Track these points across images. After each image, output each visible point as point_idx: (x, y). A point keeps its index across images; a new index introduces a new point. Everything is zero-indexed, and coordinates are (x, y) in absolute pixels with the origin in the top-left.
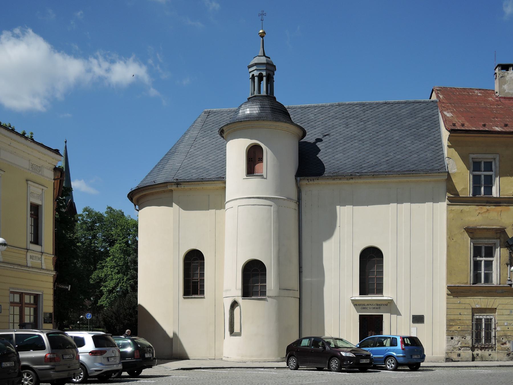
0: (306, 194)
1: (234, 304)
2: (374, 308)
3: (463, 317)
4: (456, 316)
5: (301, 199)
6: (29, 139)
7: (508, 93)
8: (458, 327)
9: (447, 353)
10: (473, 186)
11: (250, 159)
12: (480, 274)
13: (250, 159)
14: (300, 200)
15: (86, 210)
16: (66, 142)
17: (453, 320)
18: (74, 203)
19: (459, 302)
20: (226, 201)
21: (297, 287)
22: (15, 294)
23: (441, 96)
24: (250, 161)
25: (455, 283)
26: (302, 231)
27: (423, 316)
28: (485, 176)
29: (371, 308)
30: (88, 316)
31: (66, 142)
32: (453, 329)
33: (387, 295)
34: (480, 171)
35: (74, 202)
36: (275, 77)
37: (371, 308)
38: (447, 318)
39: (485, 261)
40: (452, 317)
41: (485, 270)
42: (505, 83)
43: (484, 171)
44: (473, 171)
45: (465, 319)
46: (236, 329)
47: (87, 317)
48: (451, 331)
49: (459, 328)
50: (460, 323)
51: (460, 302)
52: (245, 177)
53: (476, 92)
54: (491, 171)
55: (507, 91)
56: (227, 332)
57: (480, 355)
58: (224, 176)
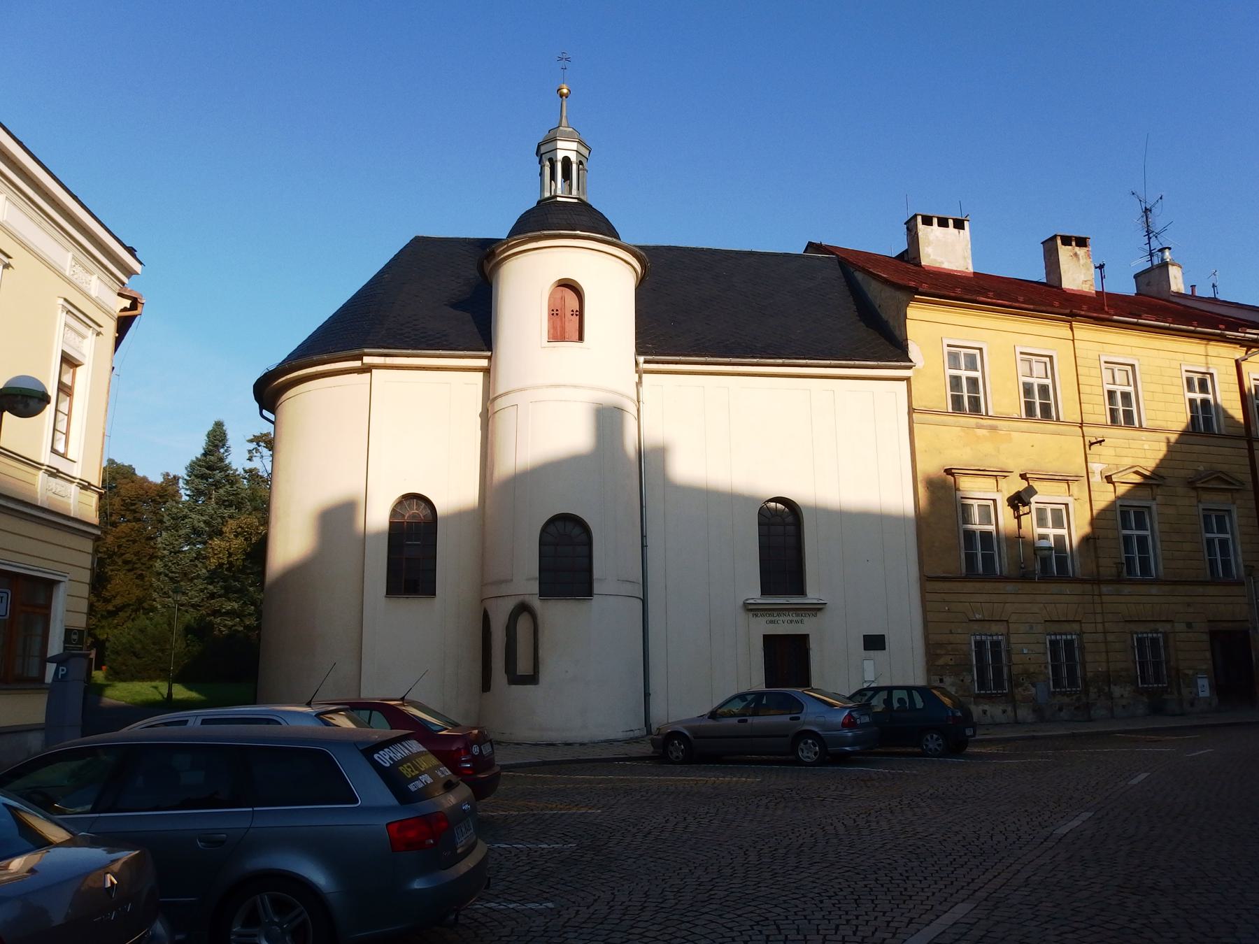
2: (791, 621)
6: (92, 487)
7: (935, 260)
8: (950, 657)
11: (553, 310)
12: (1230, 560)
19: (947, 608)
22: (1191, 294)
24: (553, 314)
27: (884, 636)
29: (786, 623)
31: (588, 349)
32: (941, 662)
37: (786, 623)
41: (1221, 556)
42: (929, 245)
46: (523, 667)
48: (938, 666)
49: (951, 660)
55: (932, 257)
57: (988, 713)
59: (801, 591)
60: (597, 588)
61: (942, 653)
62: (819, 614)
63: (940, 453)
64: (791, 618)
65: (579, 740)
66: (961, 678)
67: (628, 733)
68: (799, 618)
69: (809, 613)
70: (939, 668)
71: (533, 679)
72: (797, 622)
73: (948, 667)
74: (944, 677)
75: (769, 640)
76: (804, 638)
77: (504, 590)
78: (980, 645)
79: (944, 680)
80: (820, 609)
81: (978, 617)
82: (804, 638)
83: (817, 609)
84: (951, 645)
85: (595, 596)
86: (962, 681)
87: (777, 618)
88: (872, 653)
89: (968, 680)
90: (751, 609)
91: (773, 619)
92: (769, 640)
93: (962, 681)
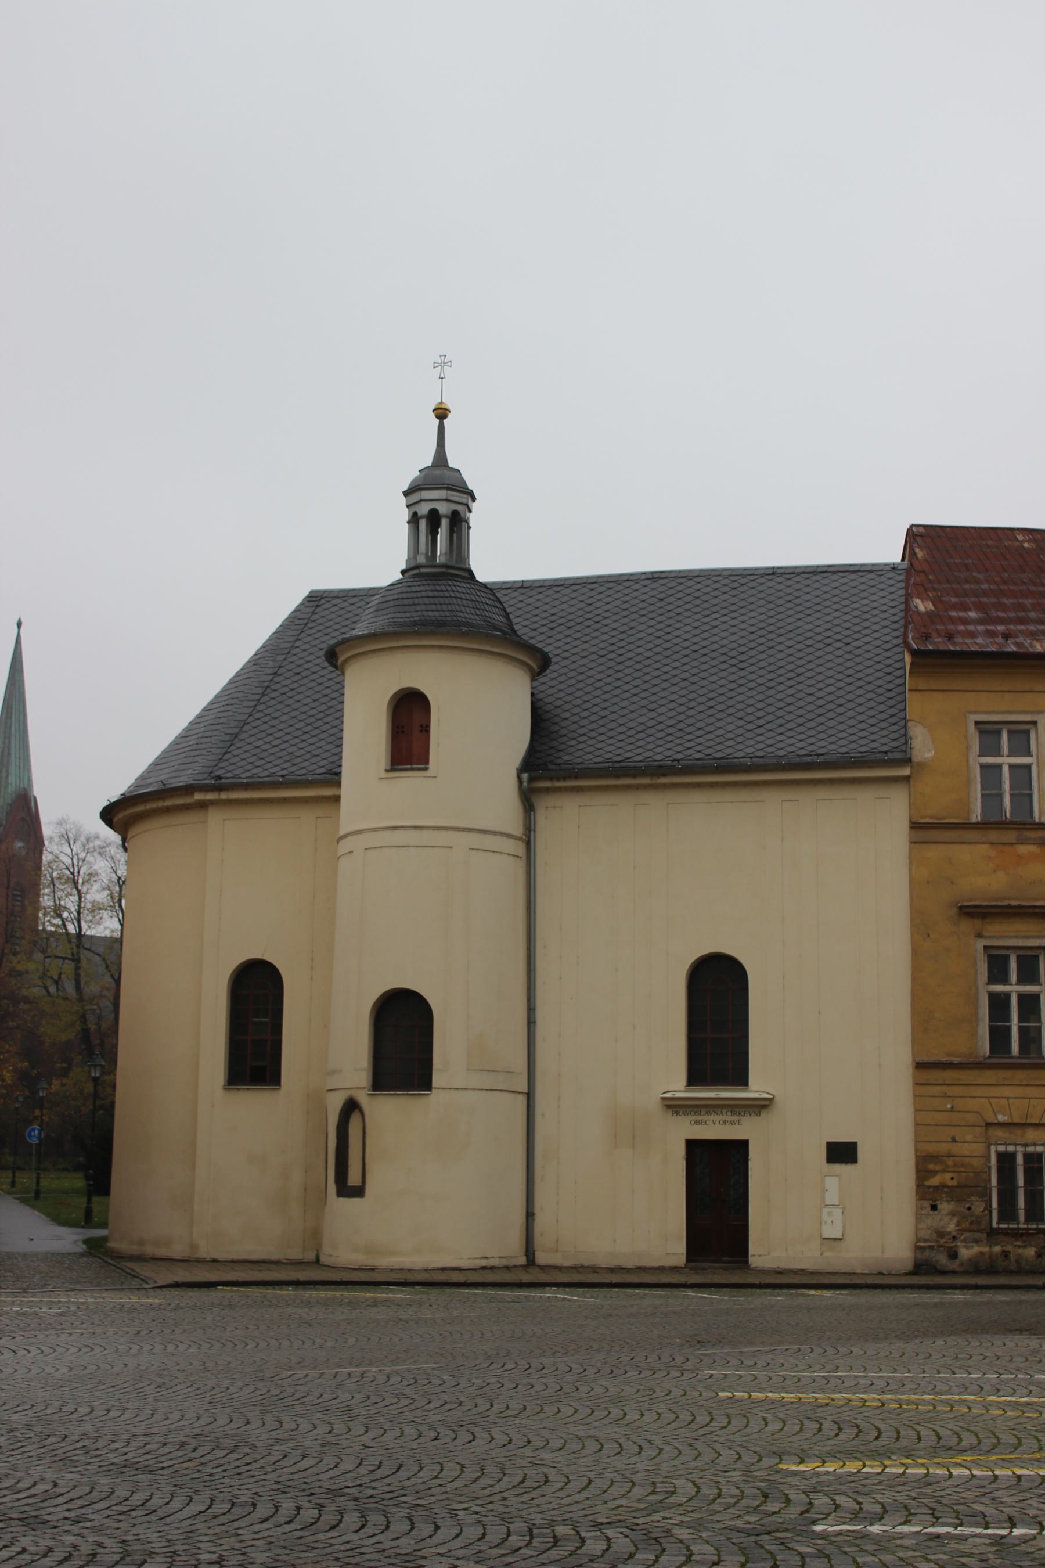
0: (546, 818)
1: (351, 1107)
2: (725, 1122)
3: (963, 1149)
4: (943, 1145)
5: (534, 831)
9: (918, 1248)
10: (1001, 789)
11: (398, 727)
13: (398, 727)
14: (532, 833)
15: (60, 823)
16: (19, 624)
17: (934, 1158)
18: (35, 798)
19: (949, 1106)
20: (342, 832)
21: (520, 1063)
23: (920, 554)
24: (398, 732)
25: (920, 1059)
26: (535, 912)
28: (1012, 767)
29: (717, 1123)
30: (33, 1134)
31: (19, 624)
32: (935, 1181)
33: (757, 1087)
34: (999, 754)
35: (35, 793)
36: (473, 519)
37: (717, 1123)
38: (916, 1151)
39: (1021, 997)
40: (932, 1148)
43: (1008, 756)
44: (979, 756)
45: (967, 1154)
46: (354, 1179)
47: (30, 1136)
48: (929, 1187)
49: (952, 1179)
50: (955, 1165)
51: (952, 1107)
52: (384, 774)
53: (1020, 537)
54: (1029, 754)
56: (332, 1188)
58: (337, 770)
59: (742, 1080)
60: (437, 1080)
61: (937, 1169)
62: (764, 1113)
63: (952, 883)
64: (724, 1117)
65: (408, 1268)
66: (967, 1205)
67: (478, 1261)
68: (735, 1118)
69: (695, 1110)
70: (931, 1189)
71: (358, 1192)
72: (732, 1123)
73: (946, 1189)
74: (938, 1203)
75: (693, 1146)
76: (743, 1146)
77: (335, 1082)
78: (1006, 1160)
79: (939, 1207)
80: (764, 1107)
81: (1001, 1118)
82: (743, 1146)
83: (761, 1106)
84: (951, 1158)
85: (433, 1090)
86: (969, 1209)
87: (706, 1118)
88: (838, 1168)
89: (978, 1207)
90: (674, 1106)
91: (699, 1118)
92: (693, 1146)
93: (969, 1209)
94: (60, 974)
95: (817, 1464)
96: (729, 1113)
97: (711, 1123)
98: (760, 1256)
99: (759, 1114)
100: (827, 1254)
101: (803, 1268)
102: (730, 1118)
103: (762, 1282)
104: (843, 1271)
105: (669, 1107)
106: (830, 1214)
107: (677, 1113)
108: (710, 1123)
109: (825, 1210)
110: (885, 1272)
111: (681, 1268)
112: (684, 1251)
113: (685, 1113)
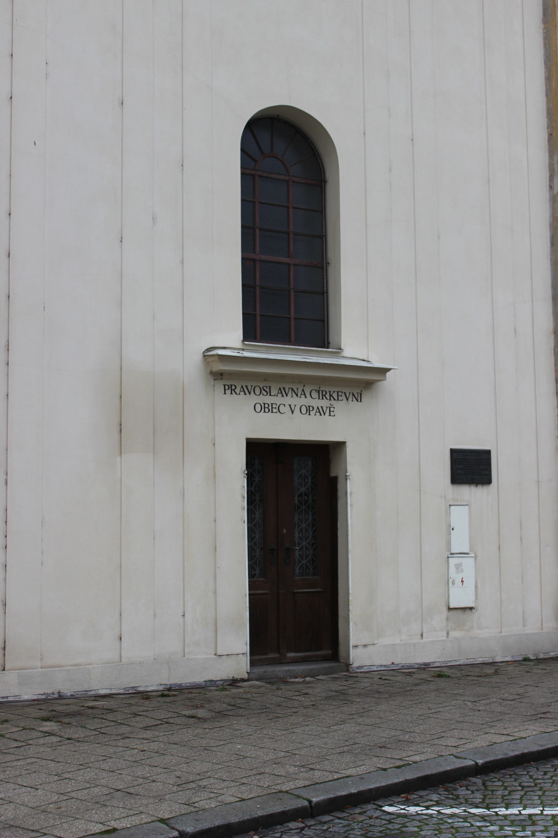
2: (309, 409)
29: (297, 410)
37: (297, 410)
64: (308, 401)
68: (324, 403)
72: (320, 411)
87: (278, 400)
91: (269, 400)
94: (436, 681)
95: (406, 807)
96: (315, 395)
97: (285, 409)
98: (365, 646)
99: (358, 398)
100: (455, 634)
101: (427, 660)
102: (317, 403)
103: (350, 595)
104: (480, 660)
105: (218, 376)
106: (458, 567)
107: (232, 389)
108: (285, 409)
109: (453, 561)
110: (532, 657)
111: (243, 680)
112: (247, 649)
113: (246, 391)
